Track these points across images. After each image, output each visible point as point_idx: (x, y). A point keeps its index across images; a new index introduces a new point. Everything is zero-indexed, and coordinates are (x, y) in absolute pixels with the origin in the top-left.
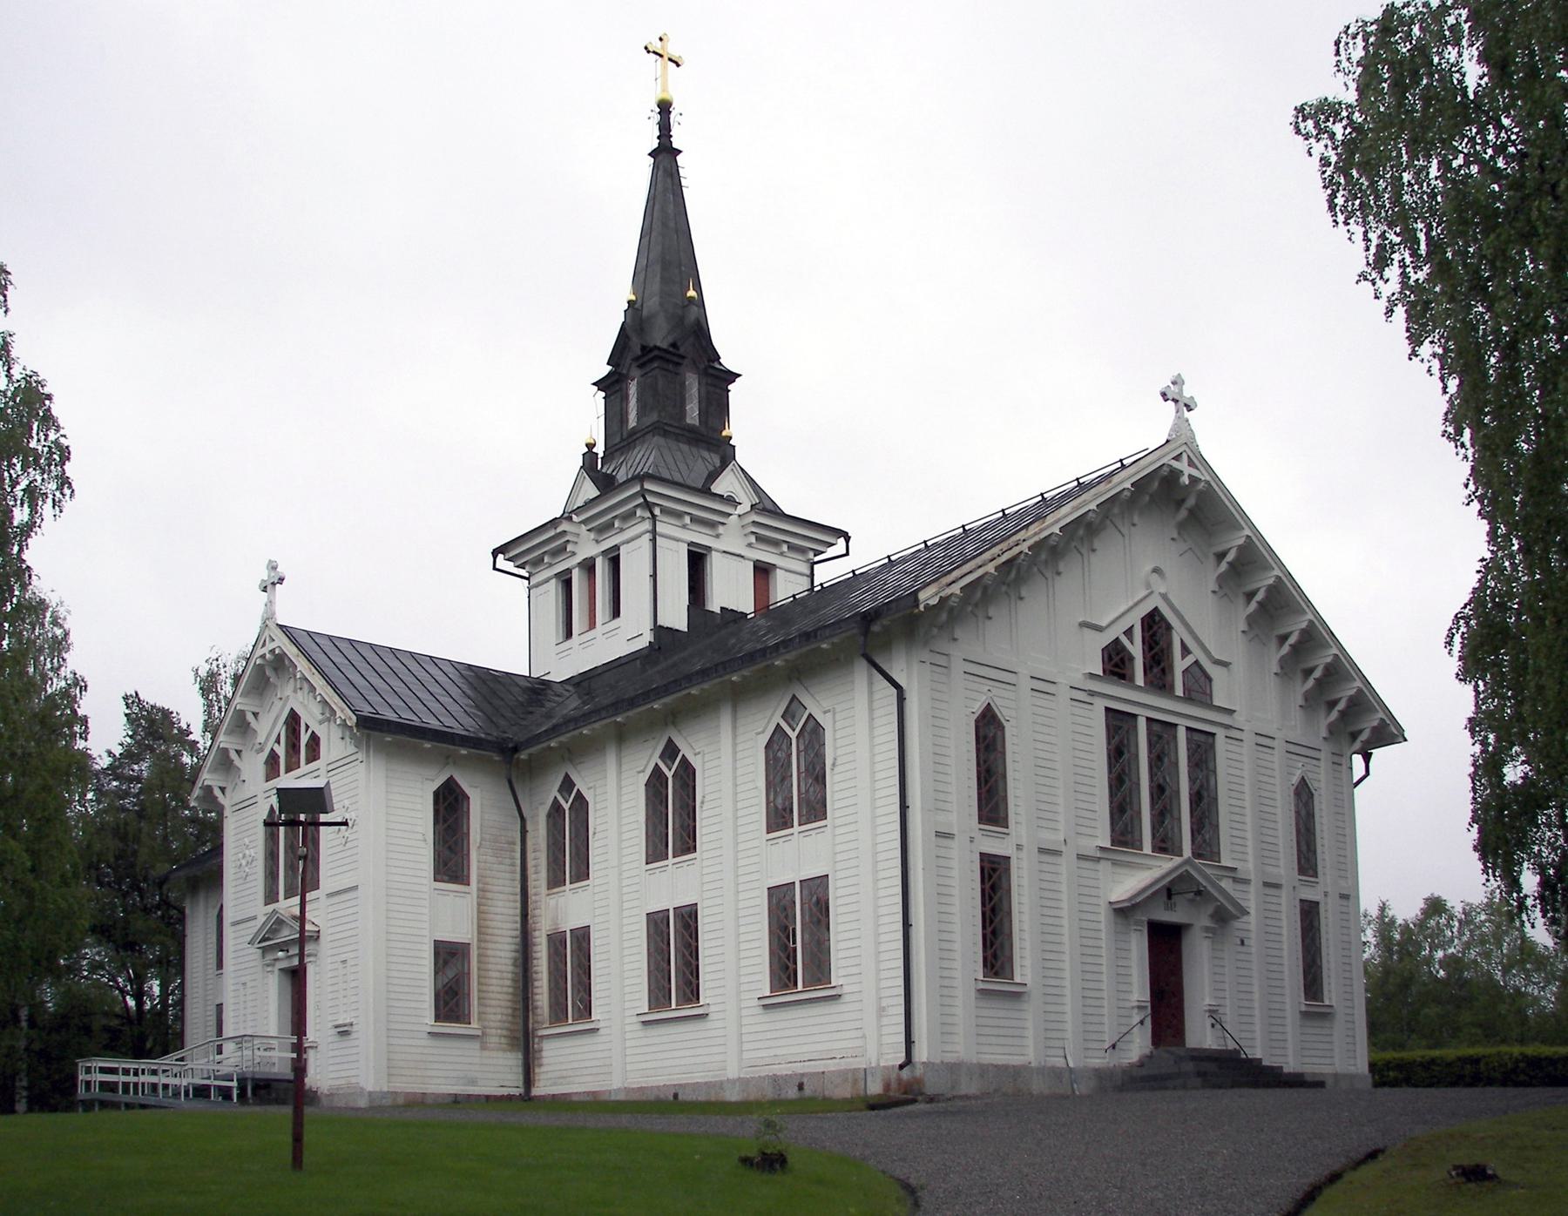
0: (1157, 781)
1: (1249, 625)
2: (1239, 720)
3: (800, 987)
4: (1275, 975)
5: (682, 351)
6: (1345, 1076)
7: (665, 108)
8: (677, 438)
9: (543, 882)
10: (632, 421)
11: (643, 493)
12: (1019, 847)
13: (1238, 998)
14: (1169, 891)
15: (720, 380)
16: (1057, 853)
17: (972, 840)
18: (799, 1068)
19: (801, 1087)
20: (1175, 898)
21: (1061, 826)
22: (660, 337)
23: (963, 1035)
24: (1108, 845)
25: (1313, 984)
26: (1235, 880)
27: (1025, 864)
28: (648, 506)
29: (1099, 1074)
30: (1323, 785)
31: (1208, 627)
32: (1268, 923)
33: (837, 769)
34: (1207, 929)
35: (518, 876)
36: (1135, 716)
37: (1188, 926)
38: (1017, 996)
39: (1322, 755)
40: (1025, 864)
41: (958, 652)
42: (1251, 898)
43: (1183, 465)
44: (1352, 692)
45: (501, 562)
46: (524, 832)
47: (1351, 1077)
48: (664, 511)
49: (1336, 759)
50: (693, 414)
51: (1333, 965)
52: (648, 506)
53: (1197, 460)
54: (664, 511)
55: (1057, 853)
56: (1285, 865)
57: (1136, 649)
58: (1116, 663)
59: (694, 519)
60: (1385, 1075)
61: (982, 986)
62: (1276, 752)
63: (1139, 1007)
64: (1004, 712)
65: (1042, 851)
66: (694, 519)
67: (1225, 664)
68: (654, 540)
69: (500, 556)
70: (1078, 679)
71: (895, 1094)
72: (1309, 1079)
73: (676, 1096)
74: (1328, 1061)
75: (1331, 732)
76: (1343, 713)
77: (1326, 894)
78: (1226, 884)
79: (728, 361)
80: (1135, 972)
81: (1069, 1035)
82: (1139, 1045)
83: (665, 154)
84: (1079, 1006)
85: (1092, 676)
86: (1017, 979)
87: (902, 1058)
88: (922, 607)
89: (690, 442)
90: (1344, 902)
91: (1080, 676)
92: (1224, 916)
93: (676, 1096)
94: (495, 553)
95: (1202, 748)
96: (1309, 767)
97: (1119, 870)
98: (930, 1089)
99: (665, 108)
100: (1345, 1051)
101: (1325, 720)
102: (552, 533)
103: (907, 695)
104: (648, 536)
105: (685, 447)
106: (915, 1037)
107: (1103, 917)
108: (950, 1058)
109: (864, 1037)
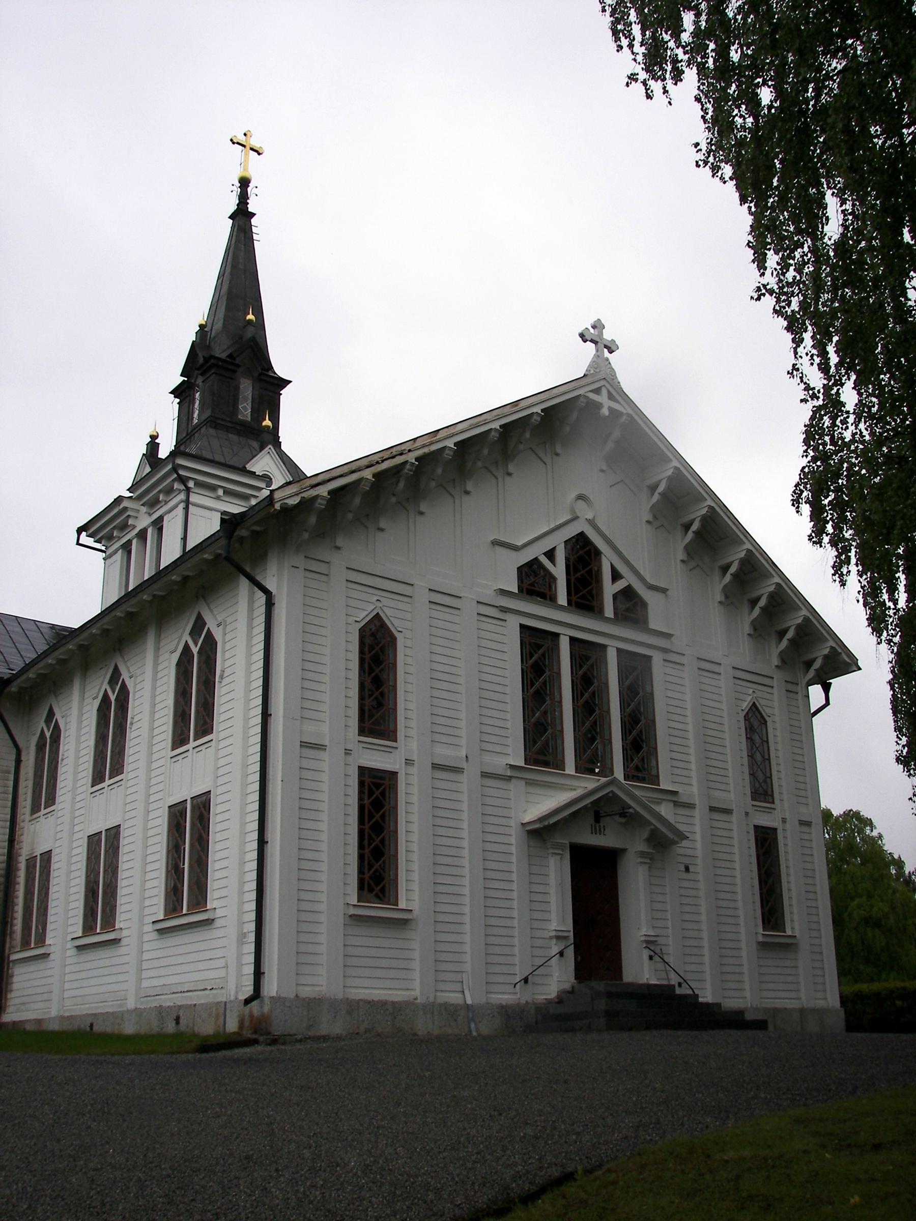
0: (579, 700)
1: (689, 554)
2: (679, 643)
3: (185, 911)
4: (540, 898)
5: (237, 361)
6: (814, 1011)
7: (244, 183)
8: (228, 429)
9: (28, 810)
10: (195, 421)
11: (175, 469)
12: (409, 762)
13: (686, 929)
14: (598, 810)
15: (272, 386)
16: (457, 770)
17: (348, 752)
18: (179, 1000)
19: (177, 1020)
20: (604, 821)
21: (463, 742)
22: (221, 352)
23: (331, 966)
24: (521, 763)
25: (772, 911)
26: (676, 804)
27: (414, 780)
28: (183, 480)
29: (504, 1010)
30: (776, 712)
31: (636, 550)
32: (716, 849)
33: (225, 681)
34: (642, 854)
35: (9, 804)
36: (557, 635)
37: (623, 851)
38: (403, 924)
39: (775, 683)
40: (414, 780)
41: (339, 562)
42: (696, 826)
43: (603, 399)
44: (799, 621)
45: (84, 539)
46: (18, 761)
47: (820, 1013)
48: (198, 484)
49: (791, 687)
50: (245, 411)
51: (794, 894)
52: (183, 480)
53: (617, 393)
54: (198, 484)
55: (457, 770)
56: (735, 789)
57: (559, 570)
58: (533, 581)
59: (227, 492)
60: (861, 1013)
61: (352, 911)
62: (722, 677)
63: (558, 938)
64: (394, 621)
65: (436, 767)
66: (227, 492)
67: (664, 591)
68: (186, 509)
69: (84, 534)
70: (488, 595)
71: (248, 1034)
72: (749, 1017)
73: (91, 1026)
74: (793, 995)
75: (783, 661)
76: (792, 641)
77: (784, 821)
78: (665, 810)
79: (280, 368)
80: (553, 899)
81: (468, 967)
82: (558, 978)
83: (242, 216)
84: (483, 933)
85: (503, 592)
86: (402, 904)
87: (249, 991)
88: (277, 506)
89: (239, 434)
90: (805, 829)
91: (492, 593)
92: (662, 842)
93: (91, 1026)
94: (80, 531)
95: (636, 670)
96: (759, 694)
97: (531, 789)
98: (277, 1029)
99: (244, 183)
100: (811, 983)
101: (776, 649)
102: (116, 511)
103: (276, 600)
104: (182, 505)
105: (234, 437)
106: (265, 968)
107: (514, 840)
108: (306, 992)
109: (226, 967)
